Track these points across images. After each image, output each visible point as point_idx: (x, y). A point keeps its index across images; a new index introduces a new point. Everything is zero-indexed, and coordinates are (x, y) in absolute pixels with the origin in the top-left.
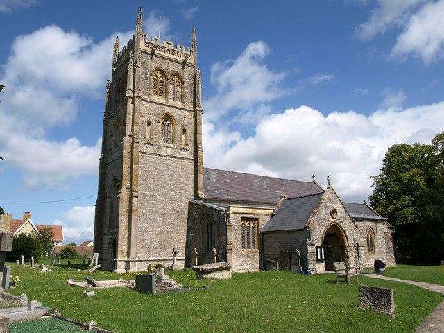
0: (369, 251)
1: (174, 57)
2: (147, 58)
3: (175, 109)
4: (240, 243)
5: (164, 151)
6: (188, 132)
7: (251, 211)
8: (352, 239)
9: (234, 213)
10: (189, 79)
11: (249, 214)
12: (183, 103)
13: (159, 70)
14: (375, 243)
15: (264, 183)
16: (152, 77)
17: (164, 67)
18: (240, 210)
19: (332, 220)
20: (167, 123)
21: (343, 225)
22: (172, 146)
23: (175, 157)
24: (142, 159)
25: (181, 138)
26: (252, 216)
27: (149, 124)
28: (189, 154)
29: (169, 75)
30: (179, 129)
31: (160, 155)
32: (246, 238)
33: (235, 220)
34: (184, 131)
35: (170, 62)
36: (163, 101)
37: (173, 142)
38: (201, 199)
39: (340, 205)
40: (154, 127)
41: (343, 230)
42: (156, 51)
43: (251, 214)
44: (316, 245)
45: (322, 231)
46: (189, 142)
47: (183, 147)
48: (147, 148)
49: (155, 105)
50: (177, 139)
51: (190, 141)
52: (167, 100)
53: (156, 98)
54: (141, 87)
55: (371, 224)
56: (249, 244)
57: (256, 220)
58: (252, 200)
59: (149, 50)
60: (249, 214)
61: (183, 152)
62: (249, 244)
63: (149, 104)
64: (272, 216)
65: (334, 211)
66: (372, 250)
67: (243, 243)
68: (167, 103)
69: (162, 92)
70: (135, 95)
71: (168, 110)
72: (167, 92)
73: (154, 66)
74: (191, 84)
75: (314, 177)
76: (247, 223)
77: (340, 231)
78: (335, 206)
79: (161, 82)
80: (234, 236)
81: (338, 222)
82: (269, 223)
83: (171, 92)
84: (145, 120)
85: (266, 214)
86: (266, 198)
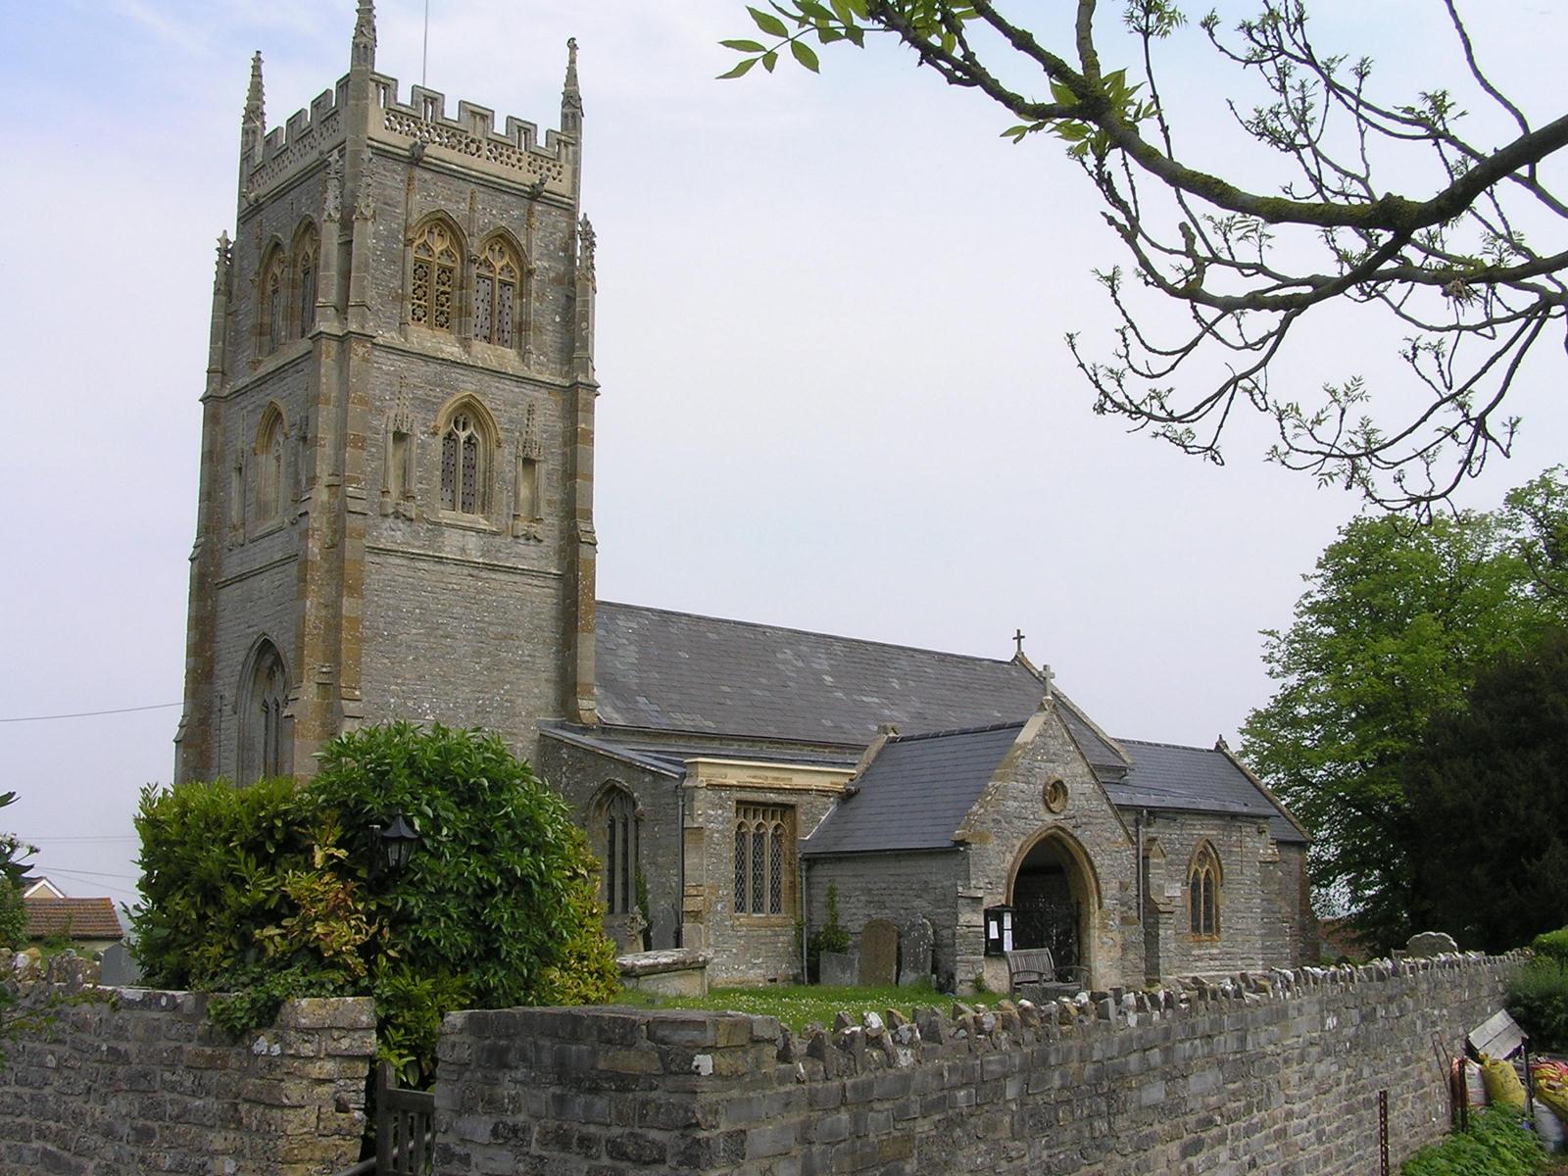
0: (1195, 928)
1: (494, 168)
2: (393, 179)
3: (494, 383)
4: (728, 891)
5: (451, 544)
6: (542, 469)
7: (768, 779)
8: (1115, 884)
9: (712, 787)
10: (550, 257)
11: (389, 145)
12: (524, 355)
13: (442, 223)
14: (1224, 901)
15: (822, 663)
16: (411, 254)
17: (458, 210)
18: (733, 777)
19: (1049, 818)
20: (463, 435)
21: (1084, 836)
22: (483, 524)
23: (493, 568)
24: (379, 574)
25: (516, 495)
26: (772, 797)
27: (400, 437)
28: (540, 557)
29: (475, 246)
30: (506, 460)
31: (440, 560)
32: (749, 873)
33: (713, 818)
34: (529, 463)
35: (482, 196)
36: (452, 350)
37: (486, 507)
38: (586, 730)
39: (1080, 768)
40: (416, 451)
41: (1086, 854)
42: (430, 149)
43: (771, 789)
44: (989, 902)
45: (1009, 858)
46: (544, 509)
47: (522, 526)
48: (393, 534)
49: (420, 367)
50: (502, 498)
51: (550, 503)
52: (465, 343)
53: (424, 338)
54: (372, 296)
55: (1208, 831)
56: (758, 895)
57: (788, 809)
58: (772, 731)
59: (400, 141)
60: (389, 145)
61: (521, 547)
62: (758, 895)
63: (401, 363)
64: (846, 797)
65: (1057, 789)
66: (1208, 928)
67: (740, 893)
68: (465, 358)
69: (445, 314)
70: (353, 327)
71: (469, 386)
72: (464, 312)
73: (420, 204)
74: (558, 281)
75: (1019, 638)
76: (774, 823)
77: (1074, 861)
78: (1059, 772)
79: (444, 270)
80: (709, 869)
81: (1068, 826)
82: (831, 821)
83: (479, 307)
84: (385, 424)
85: (824, 793)
86: (825, 728)
